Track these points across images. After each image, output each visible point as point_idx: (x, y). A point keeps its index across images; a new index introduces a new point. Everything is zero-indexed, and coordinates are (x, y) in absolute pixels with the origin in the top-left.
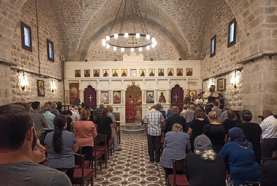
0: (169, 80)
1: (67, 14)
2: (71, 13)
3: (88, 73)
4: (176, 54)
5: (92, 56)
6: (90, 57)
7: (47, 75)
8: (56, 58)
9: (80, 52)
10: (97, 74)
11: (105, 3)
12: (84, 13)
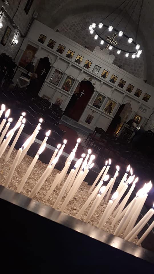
0: (124, 95)
10: (60, 50)
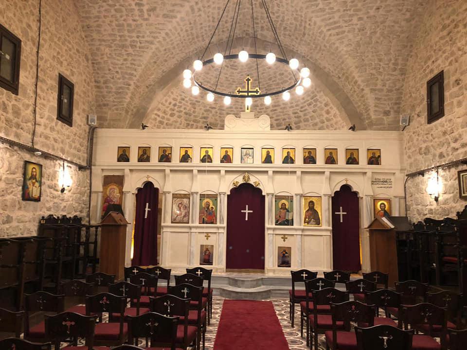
0: (327, 173)
1: (108, 28)
2: (117, 26)
3: (145, 154)
4: (339, 119)
5: (157, 121)
6: (153, 122)
7: (51, 152)
8: (78, 117)
9: (132, 110)
10: (165, 157)
11: (191, 4)
12: (144, 27)
